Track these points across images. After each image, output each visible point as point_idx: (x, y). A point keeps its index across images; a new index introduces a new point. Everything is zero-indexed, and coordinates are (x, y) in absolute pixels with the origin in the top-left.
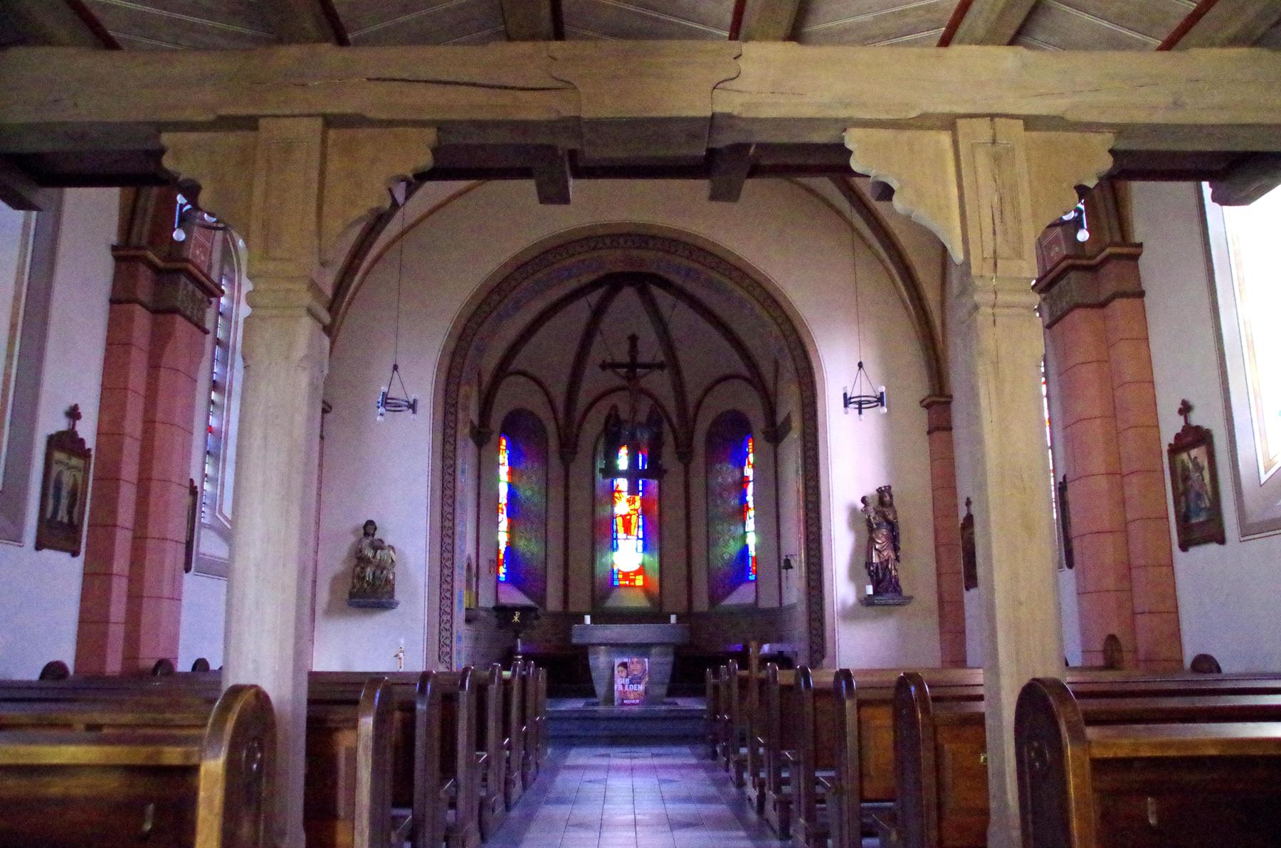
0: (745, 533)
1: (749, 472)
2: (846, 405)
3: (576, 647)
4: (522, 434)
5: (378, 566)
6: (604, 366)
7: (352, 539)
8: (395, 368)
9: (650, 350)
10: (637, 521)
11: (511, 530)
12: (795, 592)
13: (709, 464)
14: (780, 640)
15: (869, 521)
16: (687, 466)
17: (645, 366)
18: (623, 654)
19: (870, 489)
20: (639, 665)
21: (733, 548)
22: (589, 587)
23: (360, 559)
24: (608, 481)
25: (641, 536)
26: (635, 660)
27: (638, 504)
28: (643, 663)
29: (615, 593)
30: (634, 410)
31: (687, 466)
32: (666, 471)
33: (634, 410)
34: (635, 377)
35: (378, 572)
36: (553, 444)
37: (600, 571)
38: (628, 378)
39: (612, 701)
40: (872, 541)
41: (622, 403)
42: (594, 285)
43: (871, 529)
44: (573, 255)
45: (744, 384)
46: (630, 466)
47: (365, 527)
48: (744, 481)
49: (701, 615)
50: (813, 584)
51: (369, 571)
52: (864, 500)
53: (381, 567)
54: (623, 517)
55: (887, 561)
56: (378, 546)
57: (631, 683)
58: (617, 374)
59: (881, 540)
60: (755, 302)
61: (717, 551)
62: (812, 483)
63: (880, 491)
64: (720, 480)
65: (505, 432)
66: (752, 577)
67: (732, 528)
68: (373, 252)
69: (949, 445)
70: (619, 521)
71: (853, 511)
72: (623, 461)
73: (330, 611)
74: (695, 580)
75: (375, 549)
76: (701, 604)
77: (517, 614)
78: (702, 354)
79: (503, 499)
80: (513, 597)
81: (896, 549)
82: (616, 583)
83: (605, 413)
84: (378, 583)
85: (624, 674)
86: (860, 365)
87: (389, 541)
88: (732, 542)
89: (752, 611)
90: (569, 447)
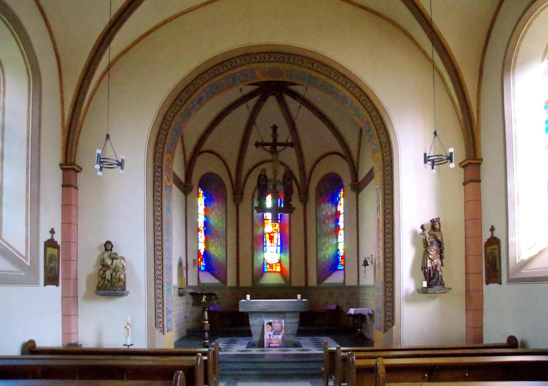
0: (338, 243)
1: (341, 208)
2: (425, 162)
3: (243, 313)
4: (212, 187)
5: (114, 270)
6: (257, 145)
7: (99, 253)
8: (108, 136)
9: (284, 135)
10: (277, 236)
11: (206, 242)
12: (369, 278)
13: (318, 204)
14: (357, 305)
17: (281, 144)
18: (269, 317)
19: (426, 220)
20: (279, 323)
23: (104, 266)
24: (261, 214)
25: (279, 244)
26: (276, 321)
27: (278, 226)
28: (281, 323)
30: (275, 172)
32: (294, 208)
33: (275, 172)
35: (114, 274)
36: (229, 192)
37: (257, 265)
38: (272, 153)
39: (263, 346)
40: (426, 253)
41: (269, 169)
42: (251, 95)
43: (426, 245)
44: (235, 67)
45: (340, 158)
46: (273, 205)
47: (105, 245)
48: (338, 214)
49: (312, 288)
50: (388, 280)
51: (108, 273)
52: (422, 227)
53: (116, 270)
54: (270, 234)
55: (436, 266)
56: (113, 258)
59: (433, 251)
60: (353, 98)
61: (321, 254)
62: (389, 216)
63: (433, 221)
64: (324, 213)
65: (200, 186)
67: (330, 240)
70: (267, 236)
71: (415, 234)
72: (269, 202)
73: (87, 297)
75: (113, 259)
76: (313, 282)
77: (204, 297)
78: (315, 138)
79: (201, 225)
80: (208, 279)
81: (441, 258)
82: (266, 270)
83: (259, 173)
84: (114, 280)
86: (435, 133)
89: (342, 288)
90: (238, 195)
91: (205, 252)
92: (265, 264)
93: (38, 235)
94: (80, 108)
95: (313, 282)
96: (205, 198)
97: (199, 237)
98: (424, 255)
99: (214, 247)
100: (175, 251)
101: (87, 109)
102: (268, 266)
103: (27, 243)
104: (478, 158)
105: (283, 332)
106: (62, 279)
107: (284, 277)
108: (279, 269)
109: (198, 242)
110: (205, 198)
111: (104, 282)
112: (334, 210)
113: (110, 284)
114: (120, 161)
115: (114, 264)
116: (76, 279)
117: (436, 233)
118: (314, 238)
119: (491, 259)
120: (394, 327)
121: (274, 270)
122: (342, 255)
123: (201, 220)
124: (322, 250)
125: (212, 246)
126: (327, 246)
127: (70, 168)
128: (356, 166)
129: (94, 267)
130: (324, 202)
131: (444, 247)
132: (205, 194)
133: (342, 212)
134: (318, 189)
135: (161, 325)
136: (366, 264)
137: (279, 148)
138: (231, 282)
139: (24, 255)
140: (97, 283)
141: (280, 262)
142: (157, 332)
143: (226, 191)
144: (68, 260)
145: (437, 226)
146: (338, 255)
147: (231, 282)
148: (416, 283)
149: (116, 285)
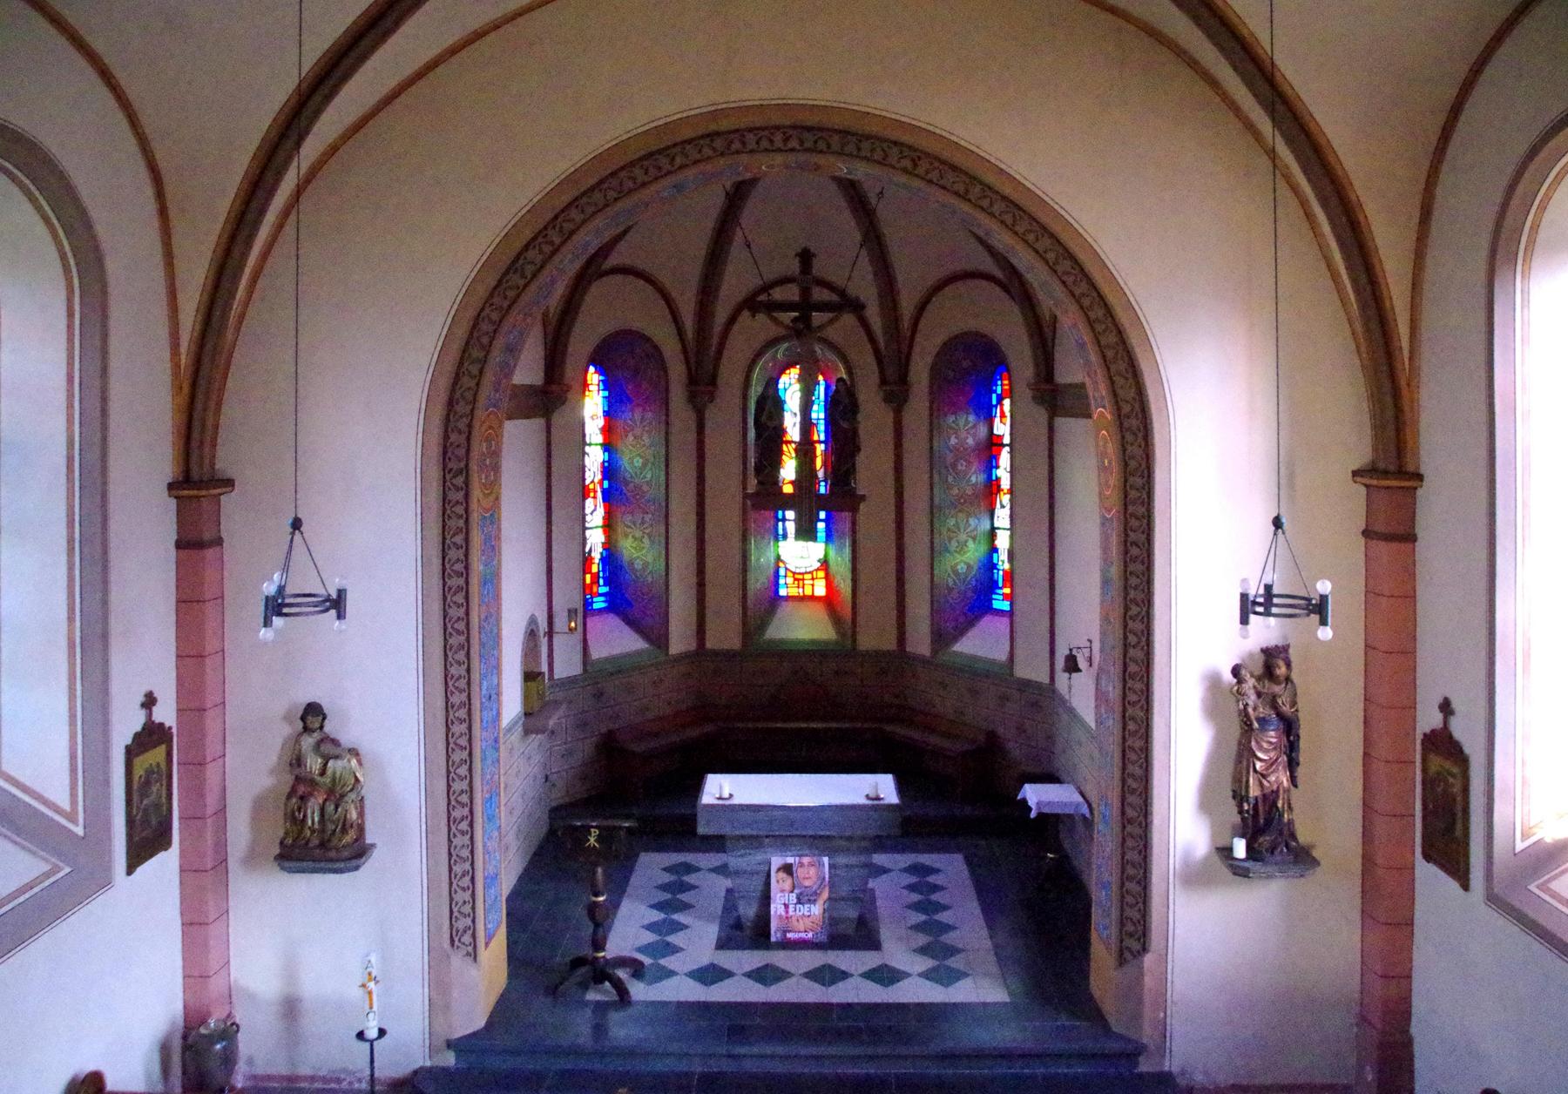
1: (1002, 429)
8: (297, 524)
11: (608, 526)
13: (935, 413)
15: (1244, 713)
16: (898, 412)
21: (973, 553)
22: (738, 609)
26: (806, 860)
28: (821, 865)
29: (785, 610)
31: (898, 412)
34: (808, 326)
35: (330, 808)
36: (677, 371)
37: (757, 582)
48: (993, 487)
51: (313, 805)
52: (1236, 671)
56: (330, 747)
57: (799, 902)
58: (775, 320)
59: (1267, 748)
66: (1000, 604)
67: (972, 521)
68: (311, 149)
69: (1408, 572)
71: (1213, 683)
73: (252, 859)
74: (910, 602)
79: (593, 473)
81: (1292, 765)
82: (783, 592)
85: (788, 884)
86: (1277, 523)
87: (347, 737)
88: (971, 544)
89: (1000, 676)
91: (610, 556)
92: (782, 572)
93: (106, 723)
94: (227, 306)
95: (920, 642)
96: (606, 393)
97: (588, 511)
98: (1238, 761)
99: (630, 540)
100: (518, 597)
101: (247, 303)
102: (790, 580)
103: (73, 770)
104: (1411, 468)
105: (825, 895)
106: (181, 818)
107: (836, 619)
108: (820, 590)
109: (585, 529)
110: (606, 393)
111: (301, 831)
112: (982, 431)
113: (318, 831)
114: (334, 596)
115: (329, 772)
116: (222, 811)
117: (1277, 689)
118: (925, 521)
119: (1438, 794)
120: (1148, 959)
121: (808, 592)
122: (1007, 566)
123: (595, 458)
124: (947, 550)
125: (626, 536)
126: (963, 537)
127: (197, 484)
128: (1049, 335)
129: (272, 772)
130: (955, 408)
131: (1302, 733)
132: (607, 385)
133: (1005, 483)
134: (935, 371)
135: (467, 938)
136: (1072, 666)
137: (818, 318)
138: (680, 640)
139: (66, 806)
140: (281, 833)
141: (825, 564)
142: (457, 961)
143: (665, 370)
144: (196, 764)
145: (1281, 670)
146: (994, 566)
147: (680, 640)
148: (1214, 835)
149: (335, 841)
